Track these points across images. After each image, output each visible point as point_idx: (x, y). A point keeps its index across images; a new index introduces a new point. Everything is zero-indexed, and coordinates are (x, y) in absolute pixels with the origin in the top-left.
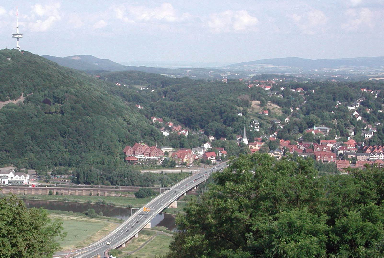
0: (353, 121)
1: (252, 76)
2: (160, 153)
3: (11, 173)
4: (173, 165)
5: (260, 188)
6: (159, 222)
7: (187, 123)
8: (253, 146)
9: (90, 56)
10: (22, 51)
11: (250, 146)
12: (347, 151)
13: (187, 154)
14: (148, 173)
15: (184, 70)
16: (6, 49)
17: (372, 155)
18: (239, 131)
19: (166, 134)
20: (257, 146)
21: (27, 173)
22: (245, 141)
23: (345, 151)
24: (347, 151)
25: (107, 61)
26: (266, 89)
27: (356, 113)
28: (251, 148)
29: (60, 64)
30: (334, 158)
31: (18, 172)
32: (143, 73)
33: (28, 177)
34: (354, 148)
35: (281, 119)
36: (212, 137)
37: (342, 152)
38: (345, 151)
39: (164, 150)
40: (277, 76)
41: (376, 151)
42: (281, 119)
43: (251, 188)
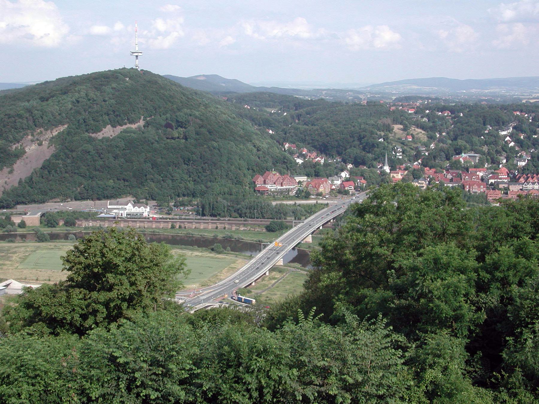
1: (394, 98)
3: (130, 205)
4: (307, 196)
6: (291, 259)
8: (395, 175)
10: (142, 70)
18: (380, 158)
19: (300, 161)
22: (387, 169)
28: (393, 177)
29: (184, 85)
31: (137, 203)
35: (427, 145)
39: (298, 179)
42: (427, 145)
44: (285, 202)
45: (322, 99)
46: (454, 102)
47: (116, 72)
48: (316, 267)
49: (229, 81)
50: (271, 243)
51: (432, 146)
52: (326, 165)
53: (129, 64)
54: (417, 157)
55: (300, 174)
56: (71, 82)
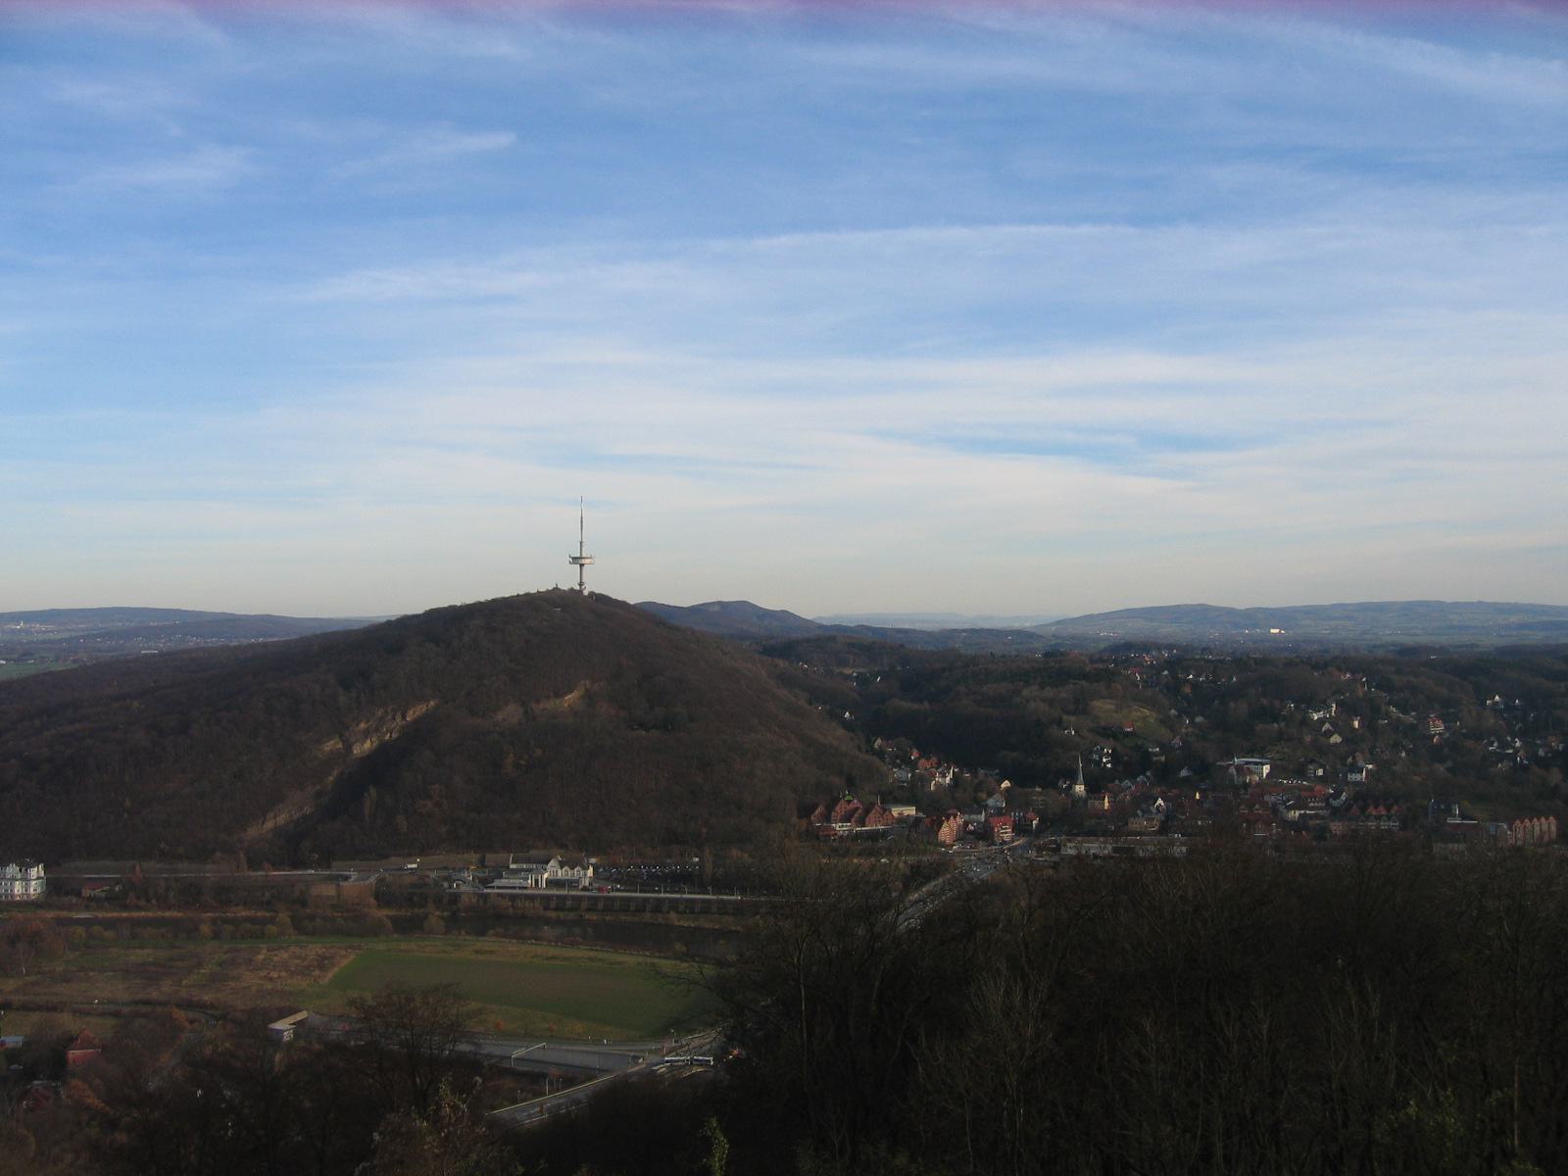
0: (1322, 750)
5: (73, 1054)
9: (743, 606)
10: (592, 594)
11: (1089, 802)
12: (1308, 812)
13: (948, 819)
17: (1362, 821)
23: (1302, 812)
24: (1308, 812)
25: (784, 616)
27: (1327, 726)
30: (1277, 827)
34: (1324, 804)
36: (1007, 782)
37: (1295, 814)
38: (1302, 812)
40: (1159, 647)
41: (1371, 810)
43: (677, 912)
53: (567, 580)
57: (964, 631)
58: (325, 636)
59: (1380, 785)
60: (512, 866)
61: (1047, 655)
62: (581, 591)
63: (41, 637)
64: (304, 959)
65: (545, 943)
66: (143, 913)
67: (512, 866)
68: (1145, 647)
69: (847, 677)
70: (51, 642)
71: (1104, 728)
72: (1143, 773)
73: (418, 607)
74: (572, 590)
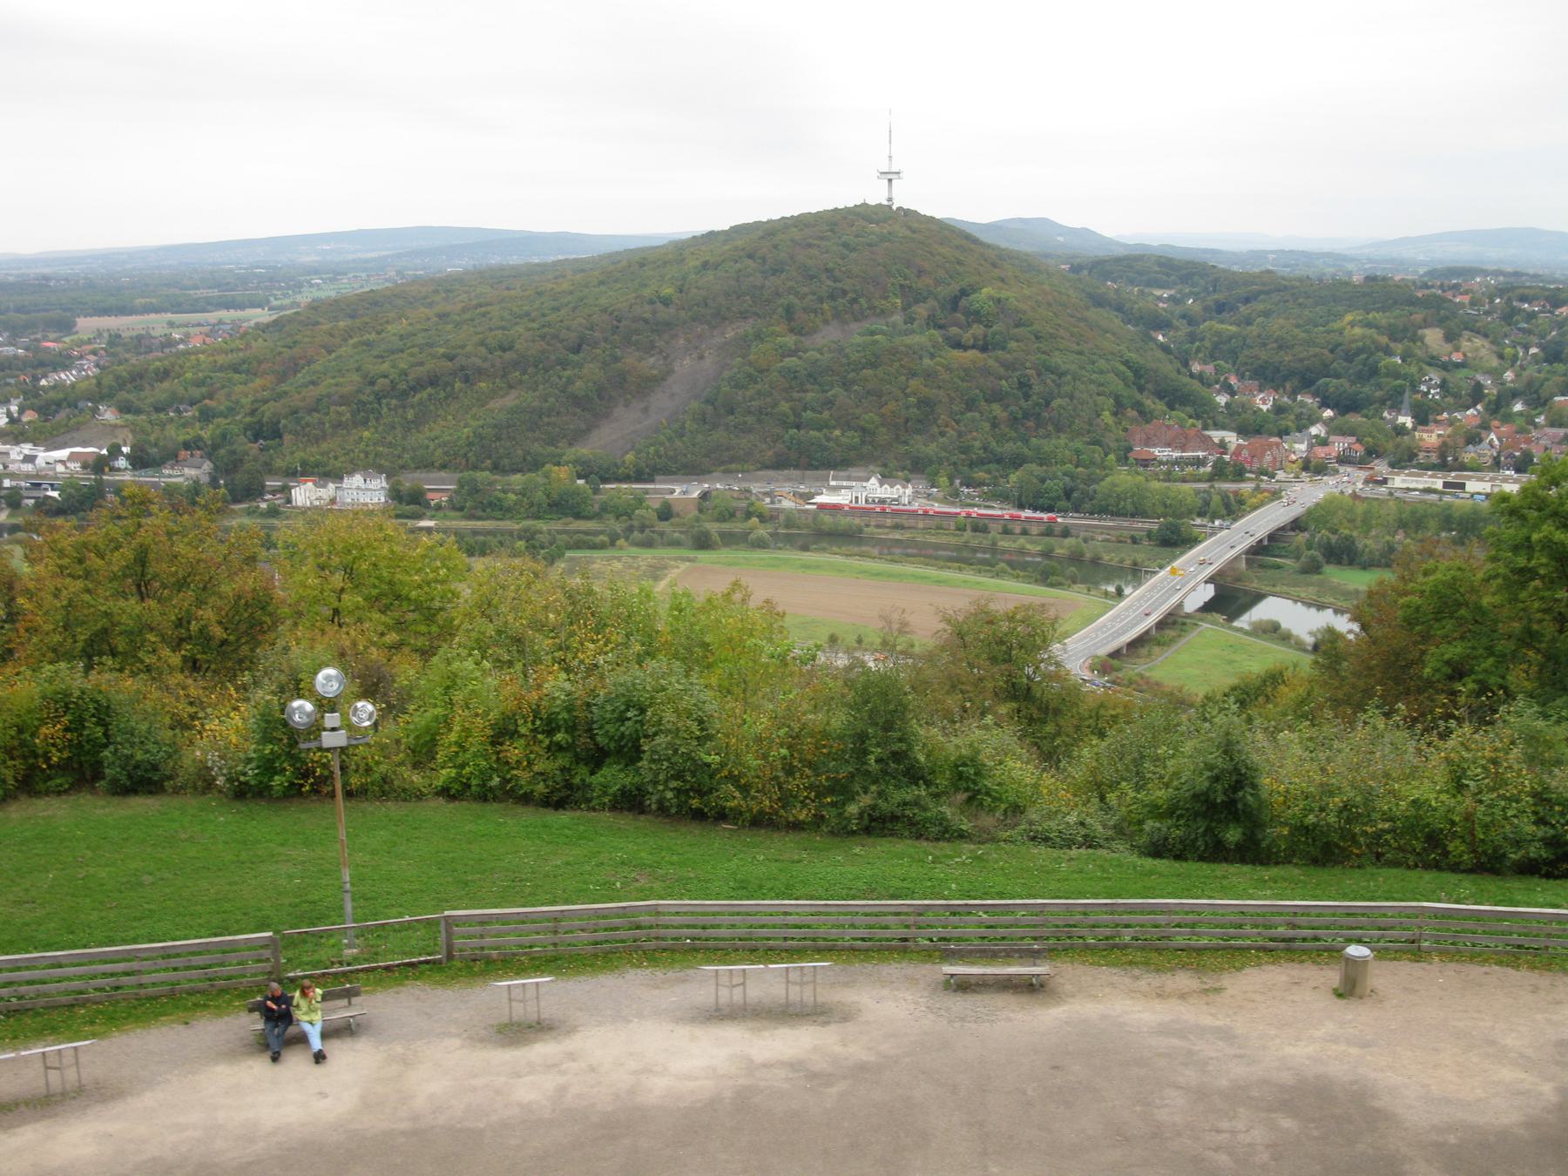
1: (1421, 271)
2: (1206, 442)
3: (873, 480)
4: (1239, 475)
6: (1201, 604)
7: (1267, 376)
8: (1425, 435)
9: (1044, 222)
10: (900, 209)
14: (233, 322)
15: (1260, 255)
16: (865, 205)
18: (1394, 401)
19: (1222, 399)
20: (1434, 436)
21: (908, 481)
22: (1407, 421)
26: (365, 491)
28: (1421, 439)
29: (985, 238)
31: (886, 478)
32: (1170, 260)
33: (909, 491)
35: (1496, 374)
39: (1216, 435)
40: (1485, 273)
42: (1496, 374)
44: (1176, 454)
45: (1269, 272)
46: (1553, 282)
47: (848, 212)
48: (1201, 826)
49: (1074, 231)
50: (1161, 567)
51: (1509, 375)
52: (1279, 410)
53: (875, 195)
54: (1477, 394)
55: (1218, 426)
56: (760, 233)
57: (1272, 252)
58: (499, 278)
59: (629, 714)
60: (833, 483)
61: (1368, 279)
62: (890, 207)
63: (350, 257)
64: (638, 569)
65: (875, 552)
66: (479, 523)
67: (833, 483)
68: (1468, 272)
69: (1160, 298)
70: (366, 261)
71: (1433, 358)
72: (1474, 405)
73: (723, 225)
74: (880, 205)
